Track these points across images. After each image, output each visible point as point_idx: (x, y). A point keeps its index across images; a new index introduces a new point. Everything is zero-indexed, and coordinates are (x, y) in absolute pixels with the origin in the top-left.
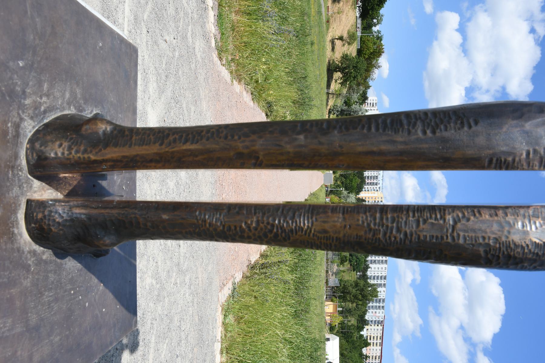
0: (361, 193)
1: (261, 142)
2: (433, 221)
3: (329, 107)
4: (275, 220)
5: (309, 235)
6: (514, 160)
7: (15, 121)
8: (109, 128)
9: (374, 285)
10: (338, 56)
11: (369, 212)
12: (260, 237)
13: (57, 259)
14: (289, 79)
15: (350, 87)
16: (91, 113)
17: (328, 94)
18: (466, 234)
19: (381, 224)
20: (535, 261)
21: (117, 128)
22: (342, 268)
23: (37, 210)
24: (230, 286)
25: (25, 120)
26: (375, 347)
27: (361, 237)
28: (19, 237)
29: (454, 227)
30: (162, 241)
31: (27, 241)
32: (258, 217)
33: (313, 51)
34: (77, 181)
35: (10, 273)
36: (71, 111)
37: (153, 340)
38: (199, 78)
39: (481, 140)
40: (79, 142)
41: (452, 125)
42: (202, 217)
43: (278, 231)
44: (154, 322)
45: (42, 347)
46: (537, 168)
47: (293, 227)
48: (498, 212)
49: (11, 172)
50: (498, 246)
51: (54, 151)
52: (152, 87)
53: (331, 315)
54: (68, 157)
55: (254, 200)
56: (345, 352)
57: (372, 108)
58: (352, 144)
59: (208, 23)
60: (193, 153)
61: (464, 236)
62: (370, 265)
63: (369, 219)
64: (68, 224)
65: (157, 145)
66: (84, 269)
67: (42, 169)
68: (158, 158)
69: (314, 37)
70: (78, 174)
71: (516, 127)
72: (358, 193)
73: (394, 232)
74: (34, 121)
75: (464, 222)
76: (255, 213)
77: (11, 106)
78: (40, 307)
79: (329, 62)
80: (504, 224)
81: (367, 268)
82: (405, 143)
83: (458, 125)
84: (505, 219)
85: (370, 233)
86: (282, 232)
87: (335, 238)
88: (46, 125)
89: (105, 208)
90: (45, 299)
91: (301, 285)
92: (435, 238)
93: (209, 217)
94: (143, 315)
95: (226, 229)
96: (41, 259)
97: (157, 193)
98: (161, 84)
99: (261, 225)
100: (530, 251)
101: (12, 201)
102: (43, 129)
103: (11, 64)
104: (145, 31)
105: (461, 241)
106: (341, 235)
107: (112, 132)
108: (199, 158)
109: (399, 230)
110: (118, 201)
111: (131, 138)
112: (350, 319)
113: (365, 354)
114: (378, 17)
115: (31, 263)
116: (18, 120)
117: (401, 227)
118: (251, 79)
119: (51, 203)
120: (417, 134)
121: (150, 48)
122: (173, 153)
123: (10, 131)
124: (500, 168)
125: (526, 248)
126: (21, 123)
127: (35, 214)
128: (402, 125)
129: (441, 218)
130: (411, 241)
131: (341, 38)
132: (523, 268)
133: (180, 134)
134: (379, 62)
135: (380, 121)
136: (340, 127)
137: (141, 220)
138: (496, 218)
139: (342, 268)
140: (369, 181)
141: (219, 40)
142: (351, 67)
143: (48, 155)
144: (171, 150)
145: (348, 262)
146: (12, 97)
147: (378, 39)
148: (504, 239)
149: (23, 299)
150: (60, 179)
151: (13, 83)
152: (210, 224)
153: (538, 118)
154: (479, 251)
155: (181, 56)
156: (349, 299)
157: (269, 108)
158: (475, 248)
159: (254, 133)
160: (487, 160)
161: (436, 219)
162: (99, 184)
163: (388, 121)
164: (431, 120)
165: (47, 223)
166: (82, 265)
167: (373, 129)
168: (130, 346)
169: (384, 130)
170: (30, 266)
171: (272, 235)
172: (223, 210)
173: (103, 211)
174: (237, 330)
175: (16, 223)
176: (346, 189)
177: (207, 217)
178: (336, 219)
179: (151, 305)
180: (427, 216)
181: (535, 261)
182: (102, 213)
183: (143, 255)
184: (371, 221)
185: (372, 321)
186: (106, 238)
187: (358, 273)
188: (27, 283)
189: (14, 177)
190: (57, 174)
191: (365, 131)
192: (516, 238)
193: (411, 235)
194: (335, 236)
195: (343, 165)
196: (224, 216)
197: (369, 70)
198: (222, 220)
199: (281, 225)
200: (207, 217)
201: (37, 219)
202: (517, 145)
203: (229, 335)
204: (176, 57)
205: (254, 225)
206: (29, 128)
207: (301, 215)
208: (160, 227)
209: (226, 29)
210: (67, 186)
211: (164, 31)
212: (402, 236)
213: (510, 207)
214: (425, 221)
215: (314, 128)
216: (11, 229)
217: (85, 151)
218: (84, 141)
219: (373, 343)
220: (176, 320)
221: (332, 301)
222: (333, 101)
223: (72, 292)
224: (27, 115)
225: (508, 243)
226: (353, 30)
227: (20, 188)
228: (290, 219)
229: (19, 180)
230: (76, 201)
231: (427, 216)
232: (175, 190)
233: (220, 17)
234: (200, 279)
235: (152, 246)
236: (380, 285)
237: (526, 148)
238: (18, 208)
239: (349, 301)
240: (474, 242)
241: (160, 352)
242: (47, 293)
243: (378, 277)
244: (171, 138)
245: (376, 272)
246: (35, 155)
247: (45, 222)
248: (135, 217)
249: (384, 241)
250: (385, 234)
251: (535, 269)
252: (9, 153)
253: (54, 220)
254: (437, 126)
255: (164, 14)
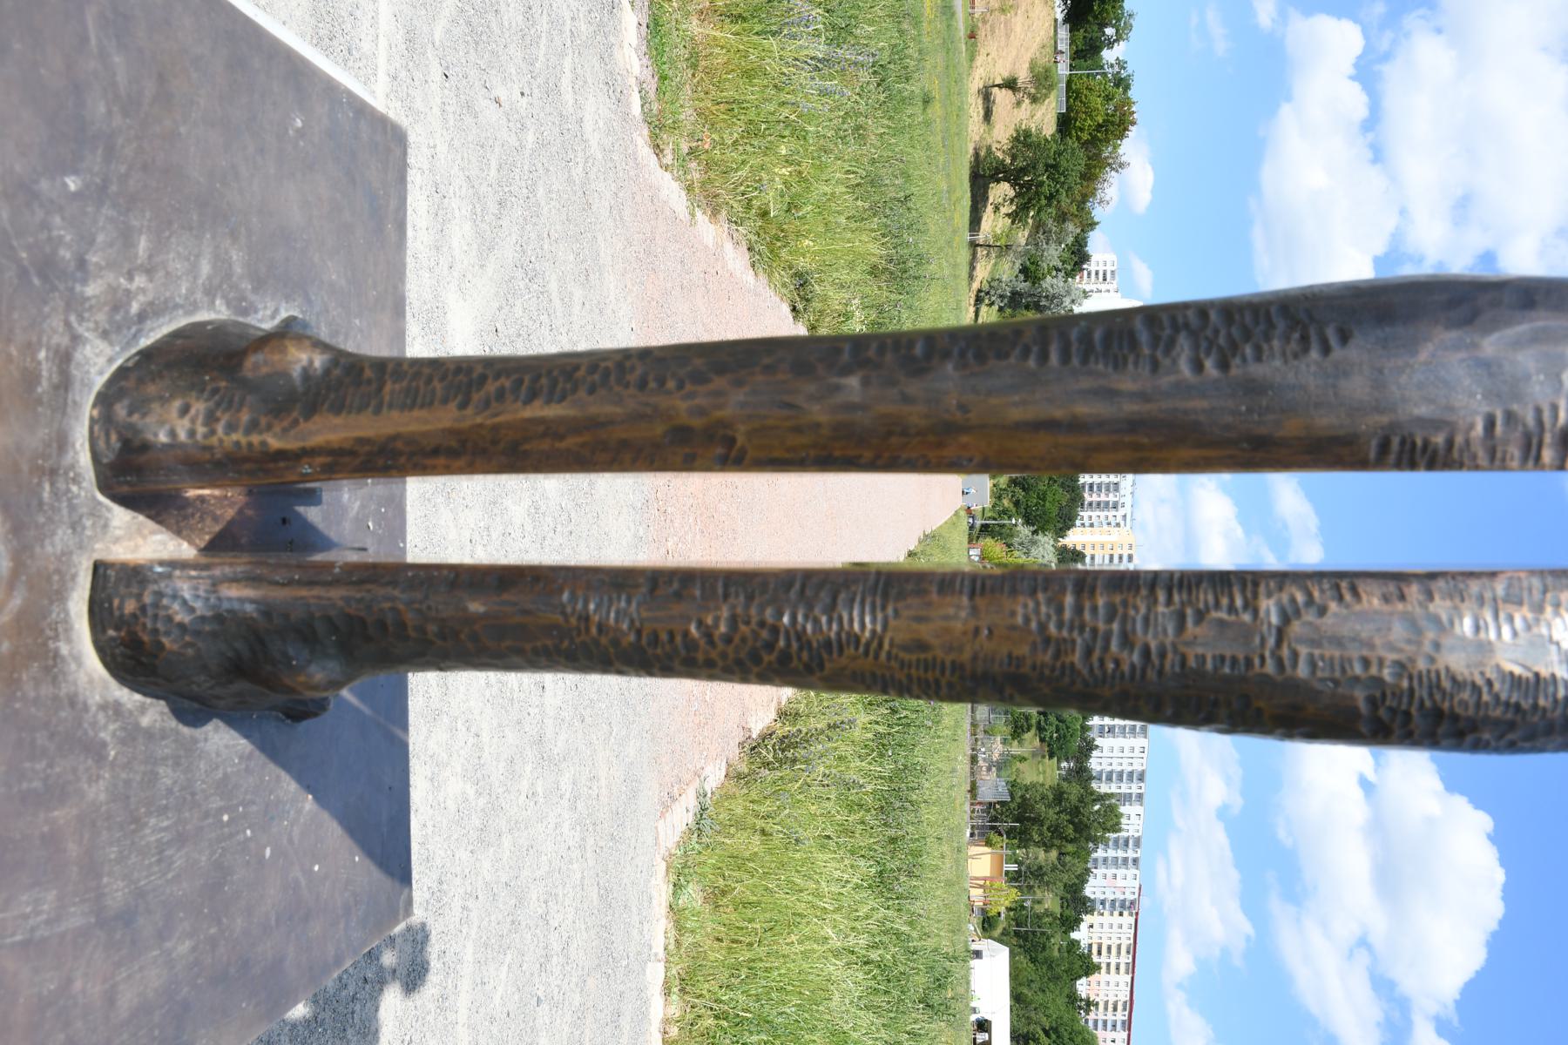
0: (1070, 533)
1: (739, 396)
2: (1223, 615)
3: (976, 286)
4: (781, 615)
5: (877, 657)
6: (1450, 443)
7: (58, 345)
8: (319, 361)
9: (1111, 795)
10: (1001, 136)
11: (1045, 590)
12: (739, 663)
13: (181, 727)
14: (859, 203)
15: (1039, 226)
16: (273, 317)
17: (974, 245)
18: (1317, 652)
19: (1077, 624)
20: (1512, 726)
21: (343, 361)
22: (1015, 749)
23: (122, 590)
24: (689, 801)
25: (84, 341)
26: (1113, 977)
27: (1020, 660)
28: (73, 666)
29: (1281, 633)
30: (493, 676)
31: (96, 676)
32: (733, 607)
33: (927, 124)
34: (237, 507)
35: (50, 765)
36: (216, 312)
37: (469, 956)
38: (594, 207)
39: (1357, 387)
40: (236, 399)
41: (1276, 343)
42: (580, 606)
43: (789, 645)
44: (471, 904)
45: (141, 969)
46: (1515, 464)
47: (833, 635)
48: (1406, 590)
49: (47, 487)
50: (1405, 684)
51: (167, 427)
52: (461, 233)
53: (986, 885)
54: (207, 442)
55: (714, 559)
56: (1025, 991)
57: (1103, 287)
58: (994, 401)
59: (621, 47)
60: (551, 430)
61: (1311, 656)
62: (1099, 741)
63: (1043, 609)
64: (207, 628)
65: (453, 406)
66: (257, 753)
67: (135, 477)
68: (454, 444)
69: (928, 80)
70: (238, 489)
71: (1457, 347)
72: (1061, 532)
73: (1114, 646)
74: (111, 344)
75: (1310, 616)
76: (726, 596)
77: (45, 302)
78: (133, 859)
79: (977, 155)
80: (1423, 623)
81: (1088, 748)
82: (1144, 397)
83: (1294, 346)
84: (1426, 608)
85: (1045, 651)
86: (801, 649)
87: (948, 664)
88: (147, 355)
89: (311, 583)
90: (150, 837)
91: (895, 800)
92: (1228, 663)
93: (598, 607)
94: (441, 883)
95: (644, 641)
96: (137, 726)
97: (476, 537)
98: (484, 226)
99: (743, 628)
100: (1497, 697)
101: (52, 567)
102: (137, 364)
103: (44, 185)
104: (436, 73)
105: (1302, 671)
106: (966, 656)
107: (327, 372)
108: (570, 442)
109: (1127, 641)
110: (346, 564)
111: (380, 389)
112: (1039, 895)
113: (1084, 996)
114: (1118, 20)
115: (108, 739)
116: (65, 341)
117: (1134, 631)
118: (749, 206)
119: (159, 569)
120: (1178, 372)
121: (451, 123)
122: (495, 428)
123: (45, 373)
124: (1413, 466)
125: (1485, 690)
126: (74, 349)
127: (116, 602)
128: (1134, 344)
129: (1246, 606)
130: (1161, 672)
131: (1010, 84)
132: (1478, 747)
133: (514, 377)
134: (1121, 151)
135: (1074, 334)
136: (962, 354)
137: (410, 618)
138: (1400, 606)
139: (1015, 749)
140: (1095, 498)
141: (652, 95)
142: (1041, 167)
143: (150, 437)
144: (489, 422)
145: (1033, 730)
146: (51, 275)
147: (1117, 85)
148: (1422, 665)
149: (87, 836)
150: (187, 503)
151: (50, 239)
152: (601, 628)
153: (1519, 323)
154: (1352, 698)
155: (542, 144)
156: (1036, 837)
157: (801, 291)
158: (1340, 690)
159: (721, 370)
160: (1374, 443)
161: (1232, 609)
162: (298, 515)
163: (1098, 335)
164: (1216, 332)
165: (149, 625)
166: (253, 743)
167: (1054, 358)
168: (402, 971)
169: (1085, 361)
170: (104, 744)
171: (773, 657)
172: (637, 586)
173: (304, 592)
174: (709, 927)
175: (63, 628)
176: (1028, 522)
177: (592, 607)
178: (951, 611)
179: (463, 854)
180: (1206, 602)
181: (1512, 726)
182: (302, 598)
183: (437, 715)
184: (1049, 616)
185: (1103, 903)
186: (313, 668)
187: (1064, 764)
188: (97, 792)
189: (58, 500)
190: (178, 490)
191: (1032, 363)
192: (1456, 661)
193: (1162, 654)
194: (949, 659)
195: (971, 460)
196: (639, 605)
197: (1092, 174)
198: (635, 615)
199: (799, 627)
200: (592, 607)
201: (122, 615)
202: (1460, 400)
203: (688, 940)
204: (529, 146)
205: (723, 628)
206: (99, 362)
207: (852, 601)
208: (462, 636)
209: (672, 62)
210: (208, 521)
211: (494, 72)
212: (1136, 657)
213: (1443, 574)
214: (1200, 616)
215: (889, 357)
216: (51, 645)
217: (253, 426)
218: (249, 398)
219: (1108, 965)
220: (534, 897)
221: (989, 843)
222: (989, 267)
223: (226, 818)
224: (91, 325)
225: (1433, 675)
226: (1044, 61)
227: (74, 528)
228: (824, 612)
229: (72, 508)
230: (231, 565)
231: (1206, 602)
232: (529, 528)
233: (655, 28)
234: (603, 782)
235: (462, 689)
236: (1127, 798)
237: (1486, 409)
238: (70, 585)
239: (1037, 844)
240: (1337, 674)
241: (488, 987)
242: (153, 821)
243: (1120, 774)
244: (491, 387)
245: (1115, 761)
246: (114, 437)
247: (144, 625)
248: (393, 609)
249: (1085, 672)
250: (1088, 652)
251: (1512, 748)
252: (43, 432)
253: (169, 619)
254: (1234, 347)
255: (494, 25)
